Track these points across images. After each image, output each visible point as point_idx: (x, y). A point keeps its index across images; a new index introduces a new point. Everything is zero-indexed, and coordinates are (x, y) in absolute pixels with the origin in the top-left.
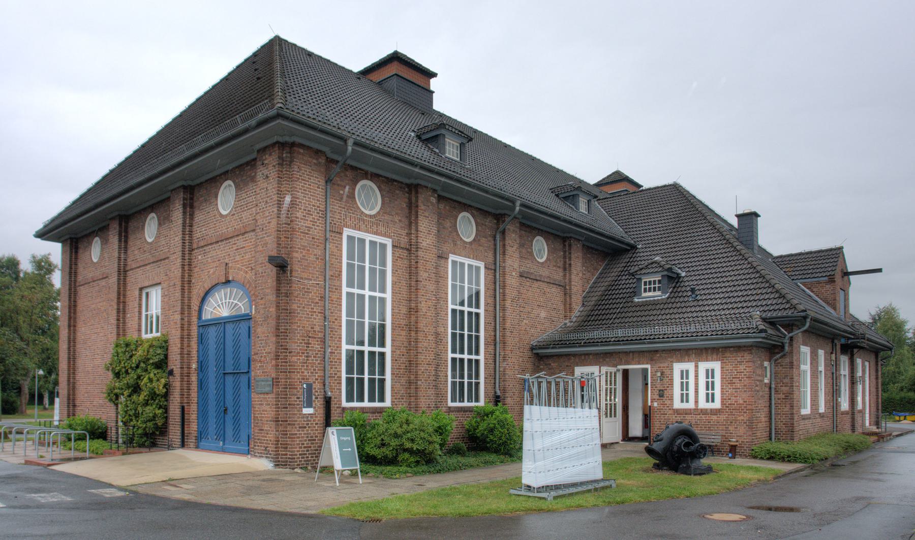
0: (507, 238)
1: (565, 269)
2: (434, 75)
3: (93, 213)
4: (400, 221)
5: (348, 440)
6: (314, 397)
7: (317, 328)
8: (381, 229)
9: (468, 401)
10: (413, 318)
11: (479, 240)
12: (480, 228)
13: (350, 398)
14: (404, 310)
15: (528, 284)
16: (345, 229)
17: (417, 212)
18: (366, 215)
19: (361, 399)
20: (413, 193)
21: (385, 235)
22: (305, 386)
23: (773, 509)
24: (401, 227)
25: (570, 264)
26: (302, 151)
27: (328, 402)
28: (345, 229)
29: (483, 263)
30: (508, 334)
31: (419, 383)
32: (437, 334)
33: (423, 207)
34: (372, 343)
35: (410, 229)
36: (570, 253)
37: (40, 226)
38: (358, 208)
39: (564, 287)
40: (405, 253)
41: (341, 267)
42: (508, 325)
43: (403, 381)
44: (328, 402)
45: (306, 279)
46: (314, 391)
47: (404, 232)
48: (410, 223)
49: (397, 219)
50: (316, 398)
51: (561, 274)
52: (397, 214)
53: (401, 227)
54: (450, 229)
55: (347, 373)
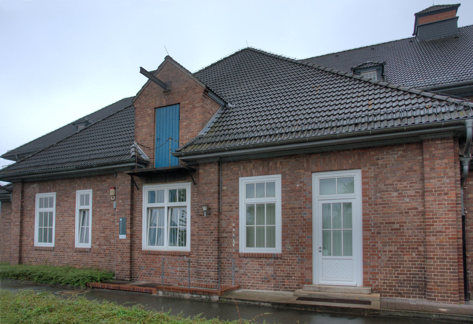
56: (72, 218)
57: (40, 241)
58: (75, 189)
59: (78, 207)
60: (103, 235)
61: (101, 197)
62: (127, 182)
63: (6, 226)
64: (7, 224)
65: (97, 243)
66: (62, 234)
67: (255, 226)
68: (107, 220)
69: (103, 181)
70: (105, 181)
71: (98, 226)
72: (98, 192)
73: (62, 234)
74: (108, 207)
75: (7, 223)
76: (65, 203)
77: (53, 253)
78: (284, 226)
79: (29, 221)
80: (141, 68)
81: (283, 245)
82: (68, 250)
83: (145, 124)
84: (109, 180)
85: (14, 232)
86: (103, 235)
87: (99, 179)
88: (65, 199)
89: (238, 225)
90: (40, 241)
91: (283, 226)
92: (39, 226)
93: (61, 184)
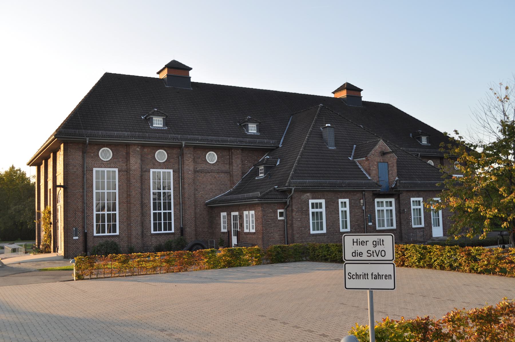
0: (184, 157)
1: (230, 164)
2: (191, 69)
3: (35, 159)
4: (122, 160)
5: (133, 253)
6: (78, 233)
7: (79, 208)
8: (113, 165)
9: (164, 230)
10: (129, 198)
11: (169, 160)
12: (169, 155)
13: (98, 232)
14: (125, 196)
15: (203, 175)
16: (94, 168)
17: (129, 156)
18: (104, 161)
19: (104, 232)
20: (128, 148)
21: (114, 167)
22: (74, 229)
23: (370, 276)
24: (123, 163)
25: (232, 162)
26: (71, 145)
27: (85, 235)
28: (94, 168)
29: (172, 170)
30: (187, 199)
31: (131, 224)
32: (404, 184)
33: (132, 154)
34: (165, 209)
35: (127, 163)
36: (232, 157)
37: (28, 161)
38: (101, 159)
39: (230, 173)
40: (125, 173)
41: (93, 183)
42: (186, 195)
43: (125, 224)
44: (85, 235)
45: (74, 190)
46: (78, 230)
47: (124, 165)
48: (127, 160)
49: (120, 160)
50: (80, 233)
51: (228, 167)
52: (120, 158)
53: (123, 163)
54: (151, 159)
55: (96, 223)
56: (337, 215)
57: (314, 230)
58: (338, 198)
59: (341, 209)
60: (357, 223)
61: (354, 203)
62: (370, 197)
63: (269, 222)
64: (270, 220)
65: (354, 228)
66: (331, 225)
67: (100, 202)
68: (358, 215)
69: (355, 195)
70: (356, 195)
71: (353, 219)
72: (353, 201)
73: (331, 225)
74: (358, 209)
75: (270, 219)
76: (332, 206)
77: (326, 237)
78: (424, 217)
79: (305, 218)
80: (332, 93)
81: (425, 224)
82: (337, 234)
83: (374, 169)
84: (358, 195)
85: (297, 225)
86: (357, 223)
87: (352, 194)
88: (332, 204)
89: (411, 216)
90: (314, 230)
91: (93, 170)
92: (346, 220)
93: (328, 195)
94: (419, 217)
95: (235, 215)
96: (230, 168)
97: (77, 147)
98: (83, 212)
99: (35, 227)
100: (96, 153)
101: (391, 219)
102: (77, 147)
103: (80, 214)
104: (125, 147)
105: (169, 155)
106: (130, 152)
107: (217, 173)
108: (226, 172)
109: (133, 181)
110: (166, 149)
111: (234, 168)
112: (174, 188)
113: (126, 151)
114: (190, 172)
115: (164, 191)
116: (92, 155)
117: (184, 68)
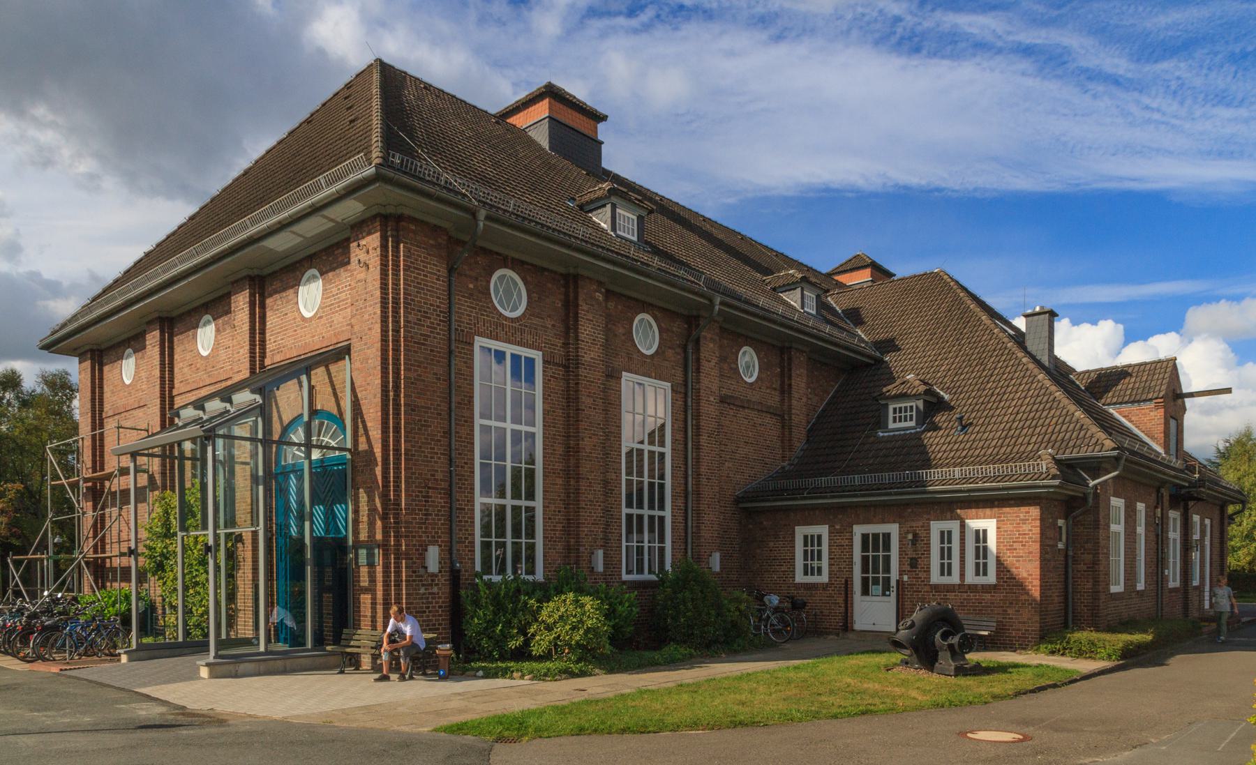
0: (702, 349)
4: (553, 325)
7: (439, 476)
14: (560, 450)
15: (731, 413)
24: (555, 334)
25: (790, 385)
30: (704, 481)
43: (560, 546)
47: (559, 342)
49: (549, 323)
52: (549, 316)
53: (555, 334)
94: (871, 554)
95: (812, 536)
96: (782, 401)
97: (431, 242)
98: (449, 493)
99: (491, 531)
100: (484, 283)
101: (520, 537)
102: (431, 242)
103: (439, 500)
104: (562, 282)
105: (665, 335)
106: (580, 303)
107: (759, 411)
108: (768, 411)
109: (586, 400)
110: (657, 313)
111: (794, 402)
112: (674, 441)
113: (562, 297)
114: (712, 399)
115: (517, 503)
116: (471, 286)
117: (612, 217)
